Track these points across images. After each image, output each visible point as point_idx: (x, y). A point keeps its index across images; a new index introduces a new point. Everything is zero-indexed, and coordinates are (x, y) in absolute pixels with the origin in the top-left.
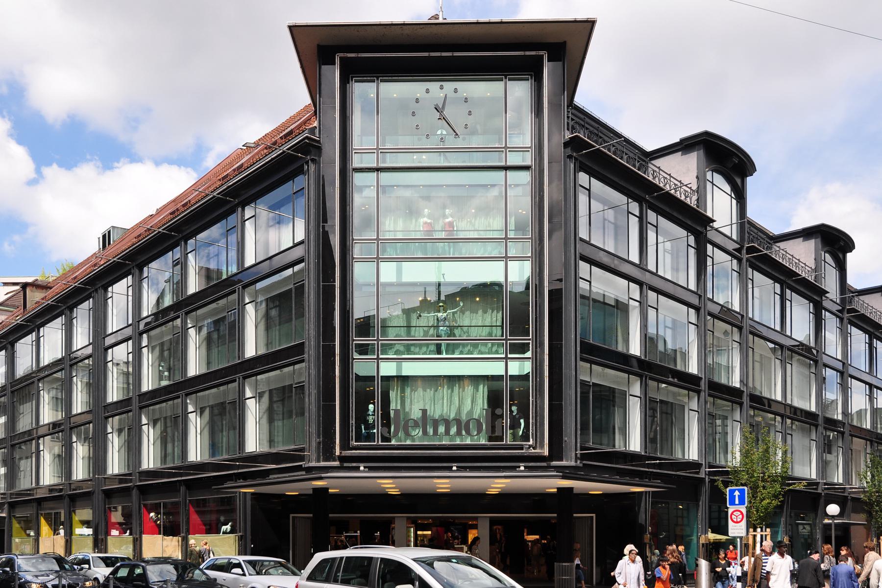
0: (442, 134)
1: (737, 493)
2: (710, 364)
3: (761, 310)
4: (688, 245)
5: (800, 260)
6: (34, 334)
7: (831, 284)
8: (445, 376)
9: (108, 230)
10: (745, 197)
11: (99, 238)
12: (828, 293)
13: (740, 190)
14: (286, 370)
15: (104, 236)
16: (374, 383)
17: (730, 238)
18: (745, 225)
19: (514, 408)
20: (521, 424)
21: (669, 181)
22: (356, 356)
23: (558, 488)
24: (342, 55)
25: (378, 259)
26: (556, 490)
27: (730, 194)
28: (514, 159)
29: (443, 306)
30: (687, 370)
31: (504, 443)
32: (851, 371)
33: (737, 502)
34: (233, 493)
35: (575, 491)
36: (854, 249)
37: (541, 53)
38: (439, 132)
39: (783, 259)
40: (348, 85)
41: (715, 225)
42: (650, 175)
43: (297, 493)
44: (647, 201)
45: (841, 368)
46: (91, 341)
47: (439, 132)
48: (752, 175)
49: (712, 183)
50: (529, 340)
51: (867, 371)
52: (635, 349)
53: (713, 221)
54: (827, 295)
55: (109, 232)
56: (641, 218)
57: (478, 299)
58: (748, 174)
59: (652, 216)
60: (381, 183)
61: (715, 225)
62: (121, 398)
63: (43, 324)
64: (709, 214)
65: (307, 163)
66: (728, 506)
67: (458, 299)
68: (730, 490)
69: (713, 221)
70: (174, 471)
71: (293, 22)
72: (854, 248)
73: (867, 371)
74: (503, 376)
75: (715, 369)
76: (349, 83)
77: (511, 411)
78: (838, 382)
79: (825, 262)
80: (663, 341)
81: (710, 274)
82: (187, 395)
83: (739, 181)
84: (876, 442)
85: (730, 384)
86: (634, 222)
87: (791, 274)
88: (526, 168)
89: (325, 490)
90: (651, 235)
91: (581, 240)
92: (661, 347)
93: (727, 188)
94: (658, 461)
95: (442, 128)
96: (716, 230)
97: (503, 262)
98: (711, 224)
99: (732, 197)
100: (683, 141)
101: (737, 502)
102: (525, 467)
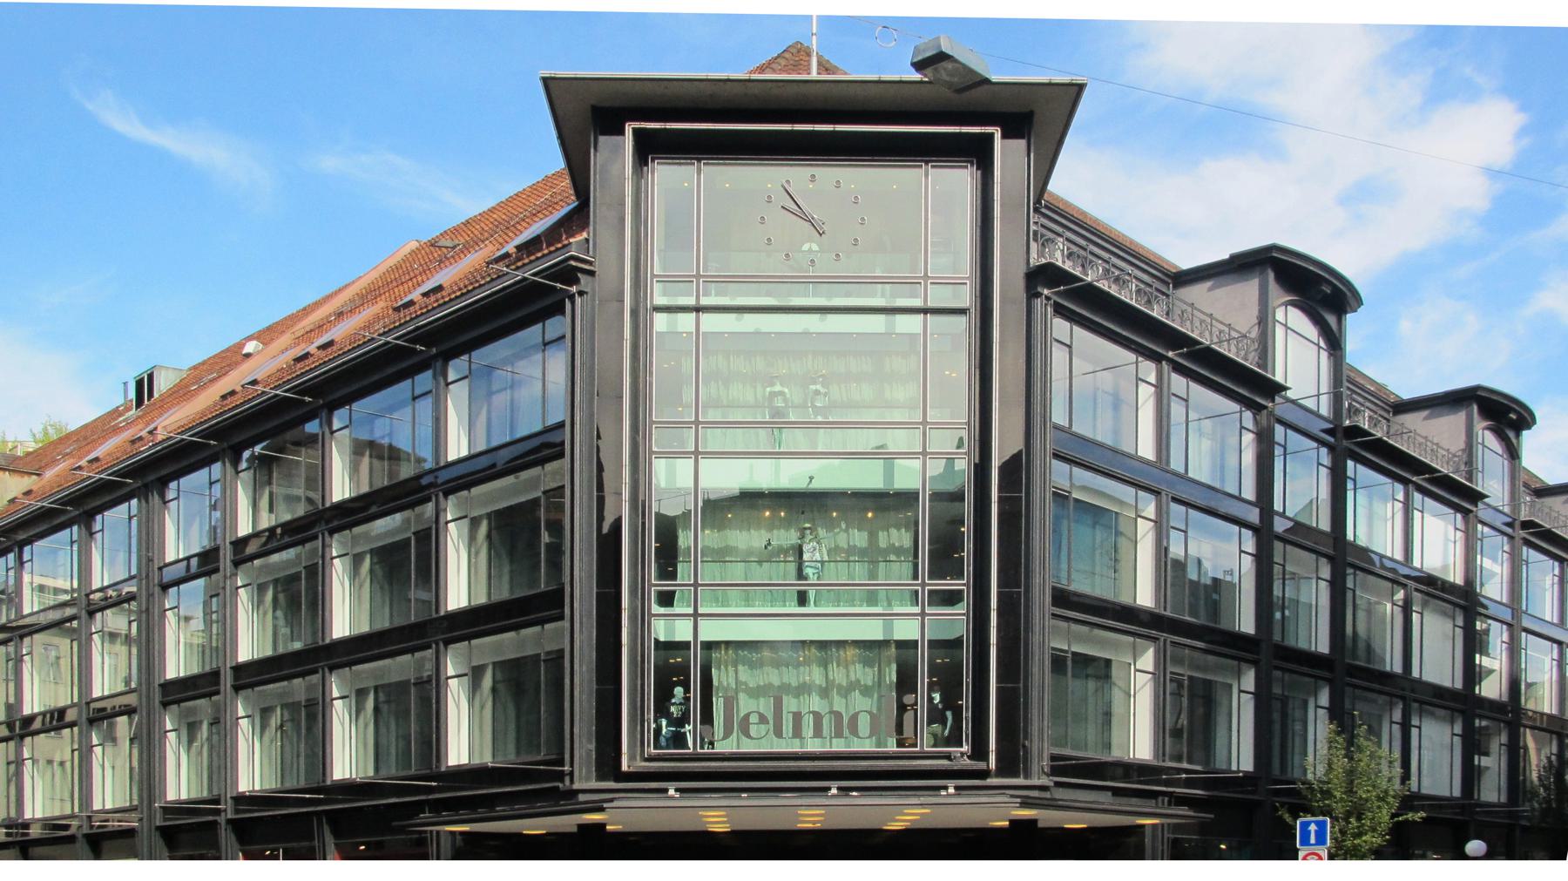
0: (810, 251)
1: (1313, 828)
2: (1278, 597)
3: (1370, 526)
4: (1242, 428)
5: (1440, 444)
6: (11, 556)
7: (1494, 484)
8: (812, 642)
9: (149, 372)
10: (1343, 346)
11: (125, 384)
12: (1487, 497)
13: (1335, 335)
14: (526, 632)
15: (139, 384)
16: (688, 652)
17: (1317, 415)
18: (1342, 378)
19: (937, 697)
20: (947, 719)
21: (1209, 327)
22: (656, 609)
23: (1011, 821)
24: (637, 125)
25: (697, 453)
26: (1007, 823)
27: (1316, 342)
28: (939, 297)
29: (809, 528)
30: (1237, 629)
31: (918, 749)
32: (1526, 623)
33: (1313, 840)
34: (421, 832)
35: (1040, 825)
36: (1535, 423)
37: (989, 129)
38: (806, 247)
39: (1408, 445)
40: (645, 168)
41: (1289, 394)
42: (1176, 317)
43: (544, 832)
44: (1169, 360)
45: (1508, 618)
46: (134, 572)
47: (806, 247)
48: (1356, 311)
49: (1286, 325)
50: (961, 585)
51: (1555, 621)
52: (1145, 597)
53: (1285, 389)
54: (1486, 500)
55: (151, 377)
56: (1159, 387)
57: (870, 515)
58: (1349, 309)
59: (1178, 382)
60: (703, 329)
61: (1289, 394)
62: (195, 670)
63: (30, 541)
64: (1279, 378)
65: (572, 298)
66: (1298, 846)
67: (835, 514)
68: (1301, 823)
69: (1285, 389)
70: (308, 796)
71: (547, 73)
72: (1534, 421)
73: (1555, 621)
74: (917, 641)
75: (1288, 617)
76: (647, 165)
77: (931, 699)
78: (1504, 640)
79: (1484, 446)
80: (1196, 565)
81: (1279, 494)
82: (332, 669)
83: (1331, 320)
84: (1415, 701)
85: (1313, 649)
86: (1146, 393)
87: (1418, 467)
88: (962, 312)
89: (601, 826)
90: (1177, 410)
91: (1057, 427)
92: (1192, 575)
93: (1311, 331)
94: (1184, 776)
95: (810, 240)
96: (1294, 402)
97: (918, 460)
98: (1284, 393)
99: (1319, 347)
100: (1235, 259)
101: (1313, 840)
102: (956, 788)
